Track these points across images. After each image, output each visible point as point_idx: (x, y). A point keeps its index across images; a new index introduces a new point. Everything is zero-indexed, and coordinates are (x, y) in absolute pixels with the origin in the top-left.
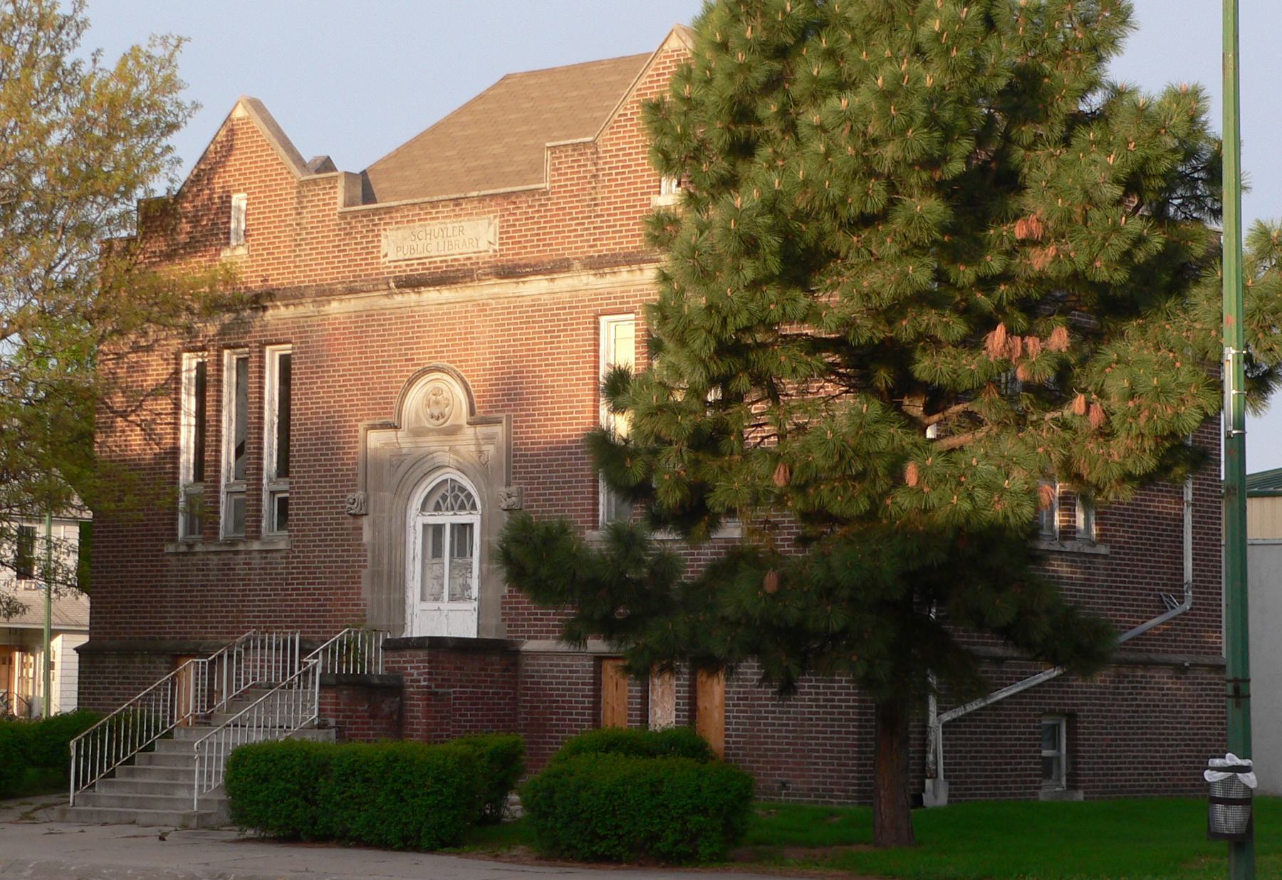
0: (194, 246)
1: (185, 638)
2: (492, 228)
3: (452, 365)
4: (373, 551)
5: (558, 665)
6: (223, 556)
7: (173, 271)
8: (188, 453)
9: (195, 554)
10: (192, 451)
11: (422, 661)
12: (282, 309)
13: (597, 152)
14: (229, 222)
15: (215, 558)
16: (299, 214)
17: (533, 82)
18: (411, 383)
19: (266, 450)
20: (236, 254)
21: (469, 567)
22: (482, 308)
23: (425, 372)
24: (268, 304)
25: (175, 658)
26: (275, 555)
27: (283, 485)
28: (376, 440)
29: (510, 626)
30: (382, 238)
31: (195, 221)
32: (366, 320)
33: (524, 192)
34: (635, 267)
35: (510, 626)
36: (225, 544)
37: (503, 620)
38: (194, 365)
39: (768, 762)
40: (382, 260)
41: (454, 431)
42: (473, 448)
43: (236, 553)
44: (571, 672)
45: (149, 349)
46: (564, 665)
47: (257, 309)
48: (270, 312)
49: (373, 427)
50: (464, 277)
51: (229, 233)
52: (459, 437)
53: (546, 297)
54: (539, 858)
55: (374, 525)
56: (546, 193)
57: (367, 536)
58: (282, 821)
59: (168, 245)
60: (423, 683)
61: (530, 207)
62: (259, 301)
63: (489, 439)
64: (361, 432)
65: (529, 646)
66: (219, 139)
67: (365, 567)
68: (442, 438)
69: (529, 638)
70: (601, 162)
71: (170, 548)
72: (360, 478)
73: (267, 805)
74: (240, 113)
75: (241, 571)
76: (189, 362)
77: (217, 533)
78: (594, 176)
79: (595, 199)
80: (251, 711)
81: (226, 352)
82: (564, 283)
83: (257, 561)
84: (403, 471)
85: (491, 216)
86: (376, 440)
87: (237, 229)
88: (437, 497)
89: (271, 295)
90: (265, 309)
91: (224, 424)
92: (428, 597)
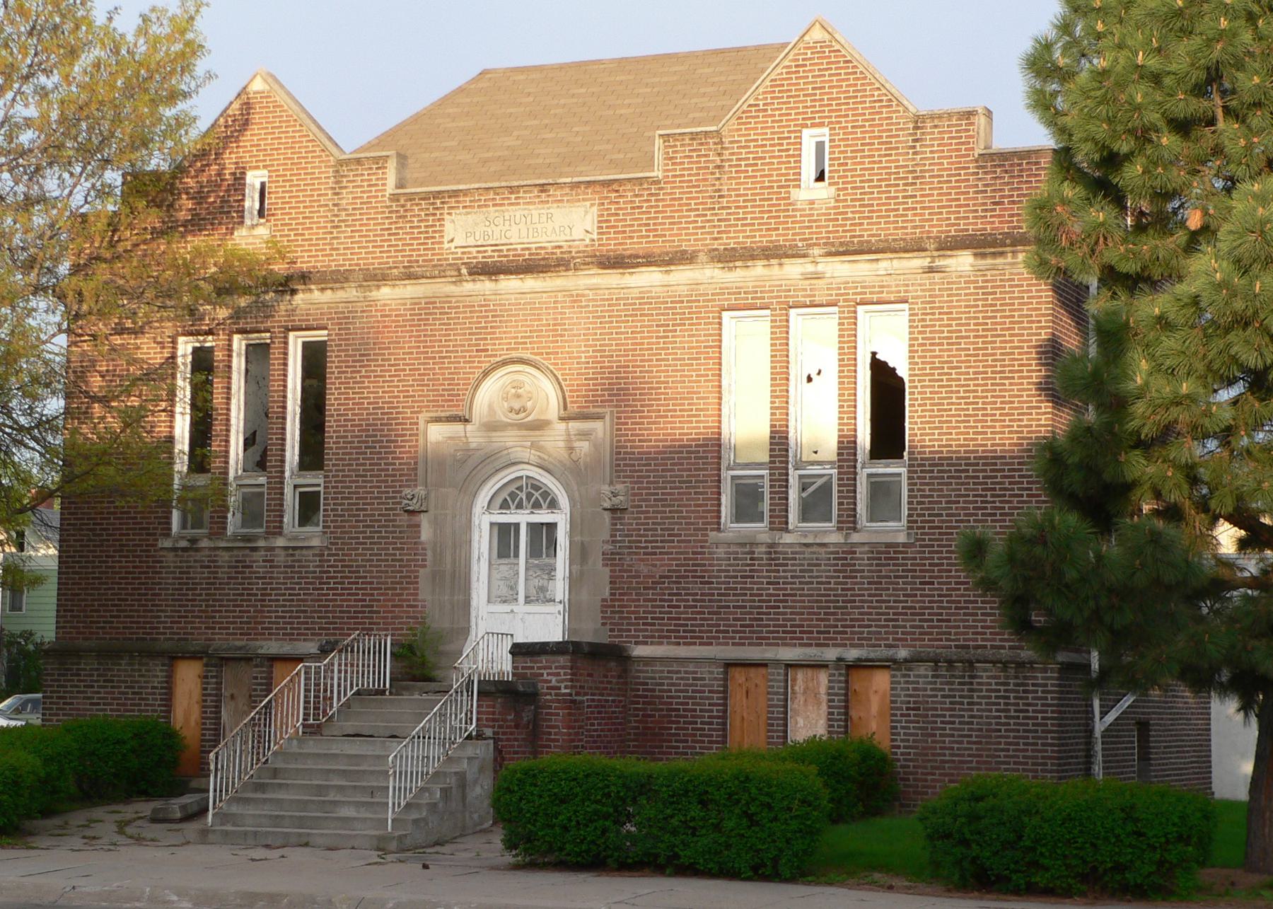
0: (196, 224)
1: (186, 639)
2: (589, 217)
3: (537, 358)
4: (434, 551)
5: (678, 672)
6: (235, 552)
7: (188, 246)
8: (183, 443)
9: (197, 550)
10: (187, 441)
11: (563, 668)
12: (317, 293)
13: (722, 143)
14: (243, 200)
15: (225, 556)
16: (337, 194)
17: (522, 77)
18: (486, 374)
19: (288, 442)
20: (251, 238)
21: (550, 571)
22: (576, 299)
23: (505, 363)
24: (299, 287)
25: (173, 658)
26: (304, 552)
27: (314, 480)
28: (436, 434)
29: (611, 630)
30: (447, 223)
31: (199, 197)
32: (426, 310)
33: (629, 180)
34: (773, 261)
35: (611, 630)
36: (235, 540)
37: (603, 624)
38: (190, 350)
39: (946, 775)
40: (446, 246)
41: (540, 425)
42: (562, 444)
43: (255, 549)
44: (694, 679)
45: (137, 332)
46: (686, 672)
47: (283, 292)
48: (299, 298)
49: (438, 420)
50: (559, 265)
51: (243, 211)
52: (546, 432)
53: (658, 289)
54: (949, 891)
55: (437, 524)
56: (658, 182)
57: (426, 534)
58: (584, 847)
59: (163, 222)
60: (564, 691)
61: (636, 196)
62: (286, 286)
63: (584, 435)
64: (421, 422)
65: (640, 651)
66: (230, 112)
67: (425, 566)
68: (525, 433)
69: (636, 643)
70: (727, 152)
71: (167, 544)
72: (420, 472)
73: (565, 829)
74: (258, 85)
75: (259, 568)
76: (185, 347)
77: (225, 528)
78: (719, 167)
79: (720, 190)
80: (429, 720)
81: (236, 337)
82: (682, 276)
83: (281, 558)
84: (468, 468)
85: (588, 203)
86: (436, 434)
87: (252, 208)
88: (505, 495)
89: (305, 277)
90: (294, 292)
91: (233, 413)
92: (493, 599)
